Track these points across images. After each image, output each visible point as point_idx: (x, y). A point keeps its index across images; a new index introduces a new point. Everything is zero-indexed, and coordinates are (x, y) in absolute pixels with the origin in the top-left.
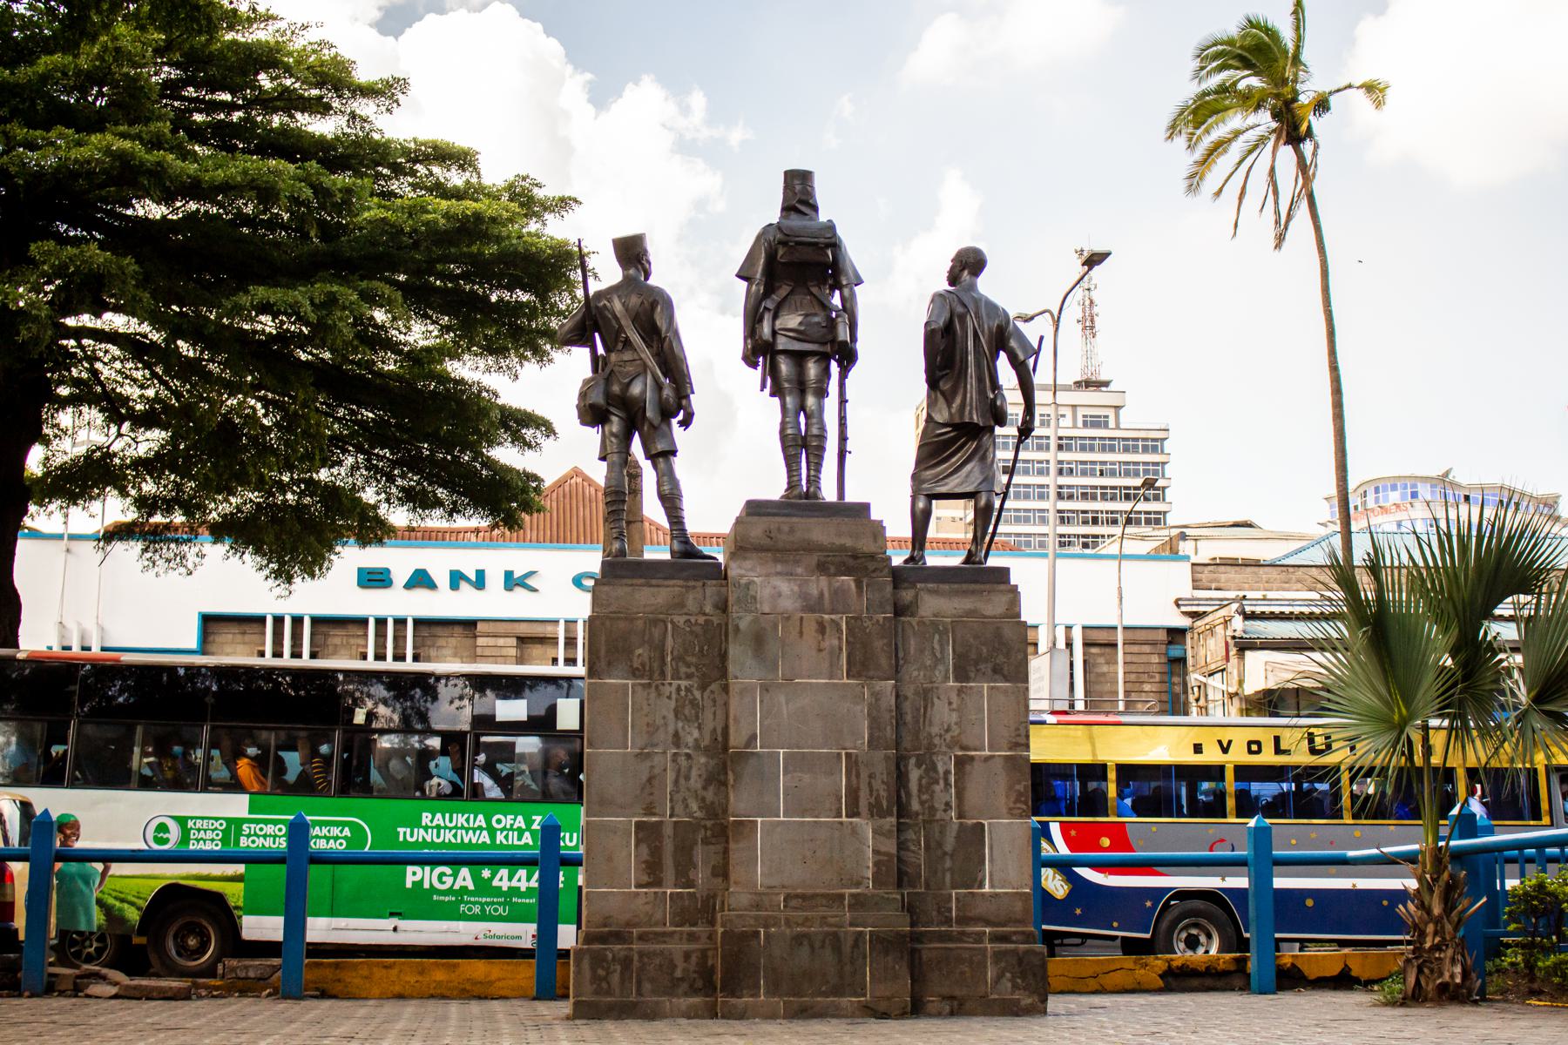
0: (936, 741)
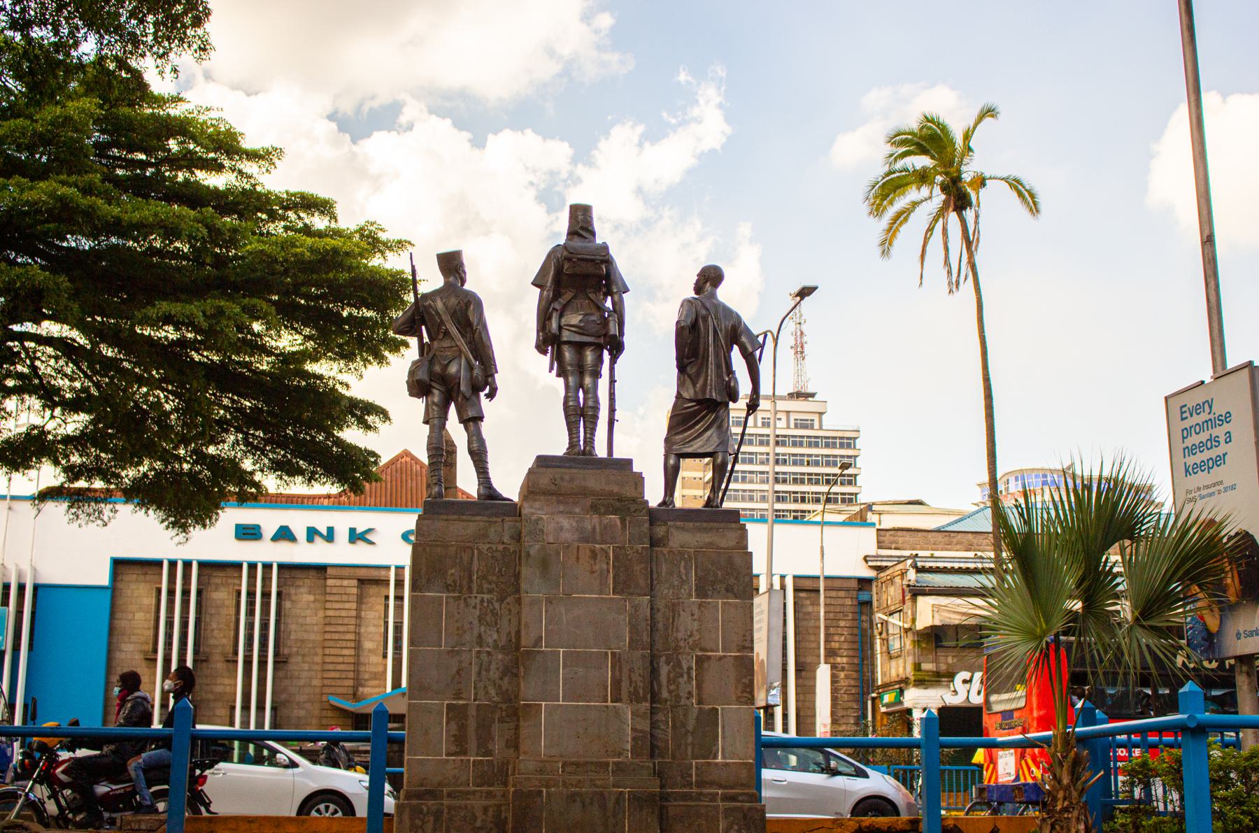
0: (682, 644)
